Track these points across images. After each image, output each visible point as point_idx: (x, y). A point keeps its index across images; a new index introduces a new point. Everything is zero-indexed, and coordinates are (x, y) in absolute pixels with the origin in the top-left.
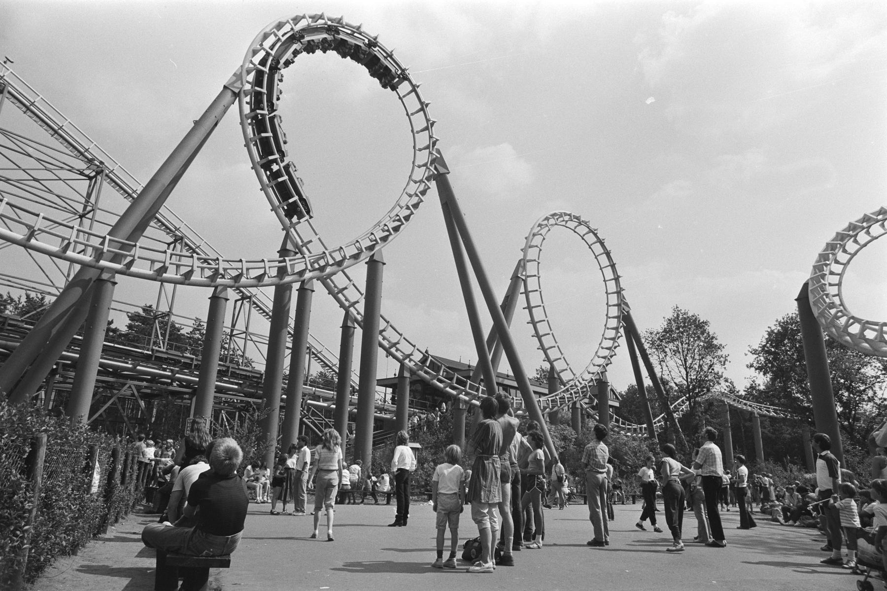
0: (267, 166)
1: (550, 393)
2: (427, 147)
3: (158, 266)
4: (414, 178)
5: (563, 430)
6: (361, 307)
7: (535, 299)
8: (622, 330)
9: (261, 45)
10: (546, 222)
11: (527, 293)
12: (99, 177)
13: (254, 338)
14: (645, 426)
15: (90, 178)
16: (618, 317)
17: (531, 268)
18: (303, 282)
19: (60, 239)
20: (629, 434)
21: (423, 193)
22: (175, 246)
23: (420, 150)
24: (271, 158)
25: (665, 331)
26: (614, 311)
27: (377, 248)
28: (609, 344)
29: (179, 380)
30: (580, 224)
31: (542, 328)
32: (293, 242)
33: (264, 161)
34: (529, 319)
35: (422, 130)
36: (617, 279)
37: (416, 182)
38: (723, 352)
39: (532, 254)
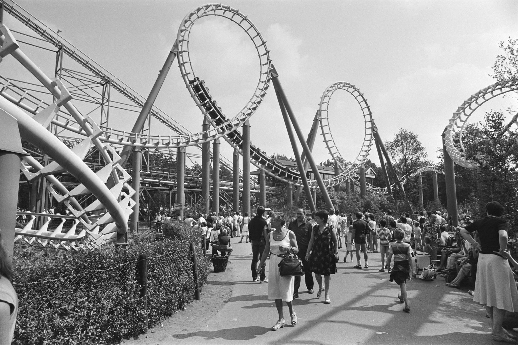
0: (204, 105)
1: (335, 175)
2: (267, 64)
4: (261, 80)
5: (341, 194)
10: (331, 89)
11: (322, 127)
12: (61, 51)
14: (386, 188)
15: (103, 85)
16: (371, 134)
17: (324, 114)
18: (215, 140)
20: (378, 193)
21: (266, 88)
22: (106, 86)
23: (263, 65)
24: (206, 102)
25: (395, 141)
26: (369, 131)
27: (246, 119)
28: (366, 148)
29: (162, 183)
31: (330, 144)
32: (208, 121)
33: (203, 103)
34: (324, 140)
35: (264, 55)
38: (424, 152)
39: (324, 107)
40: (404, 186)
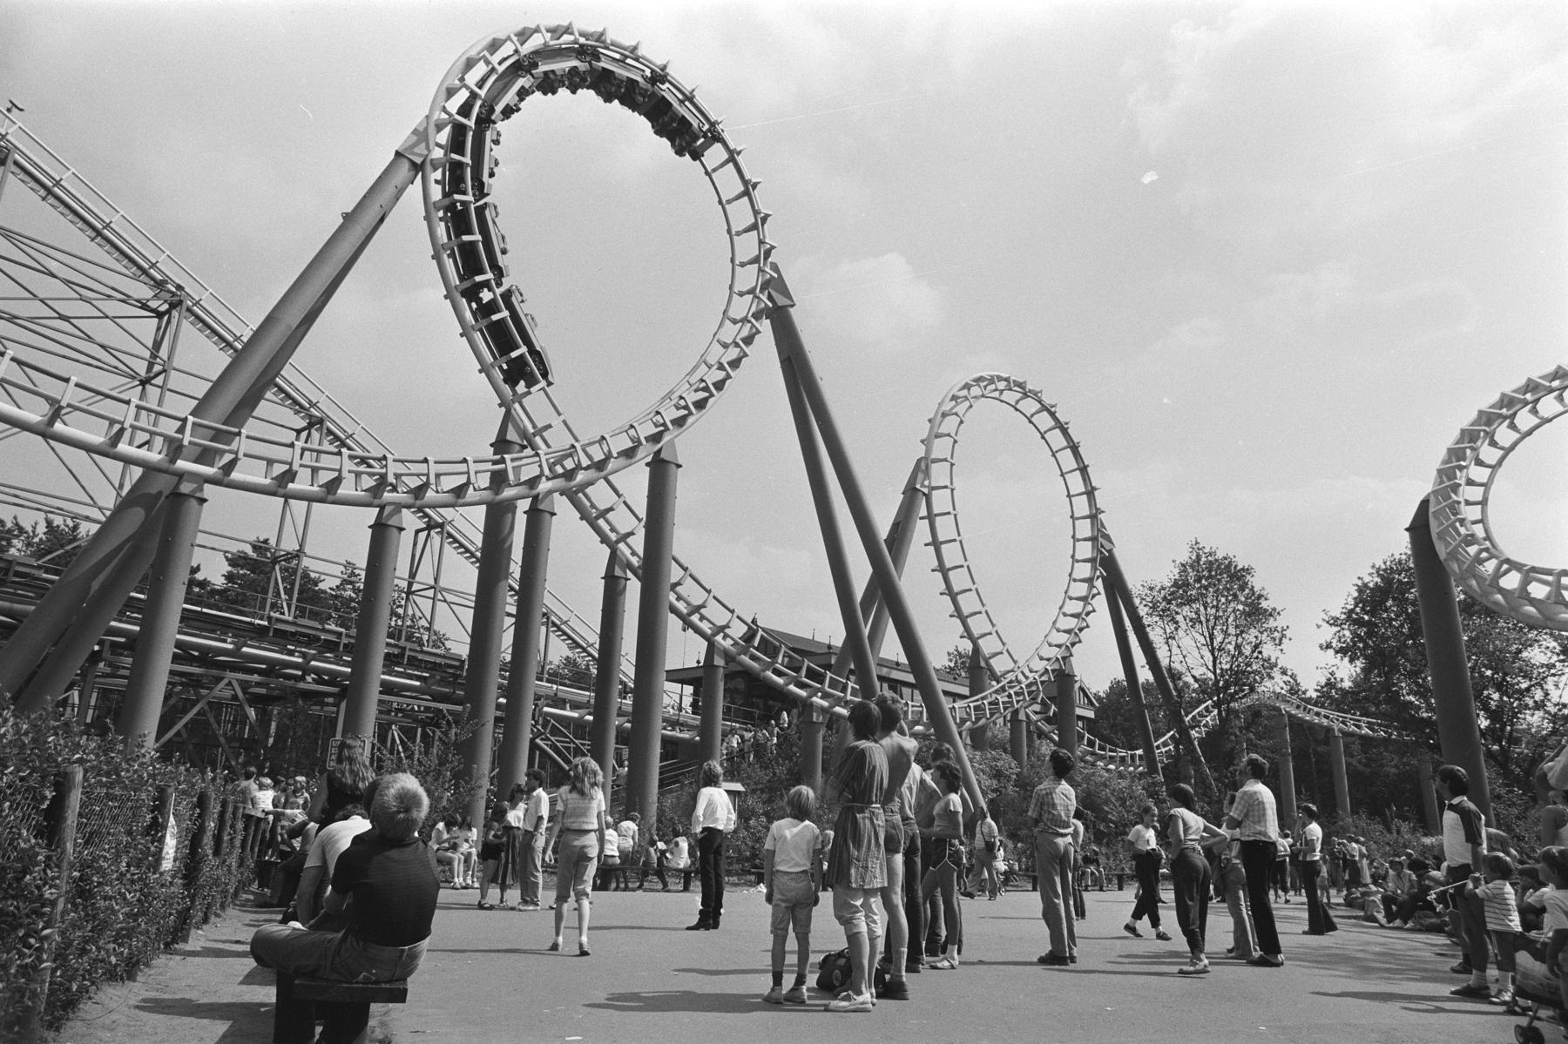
0: (472, 293)
1: (972, 694)
2: (756, 260)
3: (279, 469)
4: (731, 314)
5: (995, 759)
6: (638, 542)
7: (945, 528)
8: (1099, 584)
9: (462, 79)
10: (965, 392)
11: (931, 517)
12: (175, 313)
13: (449, 597)
14: (1140, 752)
15: (160, 315)
16: (1092, 560)
17: (939, 474)
18: (535, 498)
19: (107, 423)
20: (1112, 767)
21: (749, 340)
22: (309, 435)
23: (743, 265)
24: (478, 278)
25: (1175, 584)
26: (1085, 550)
27: (666, 438)
28: (1077, 607)
29: (317, 671)
30: (1025, 395)
31: (959, 580)
32: (517, 428)
33: (467, 284)
34: (935, 564)
35: (747, 230)
36: (1090, 493)
37: (735, 322)
38: (1278, 623)
39: (941, 448)
40: (1201, 741)
